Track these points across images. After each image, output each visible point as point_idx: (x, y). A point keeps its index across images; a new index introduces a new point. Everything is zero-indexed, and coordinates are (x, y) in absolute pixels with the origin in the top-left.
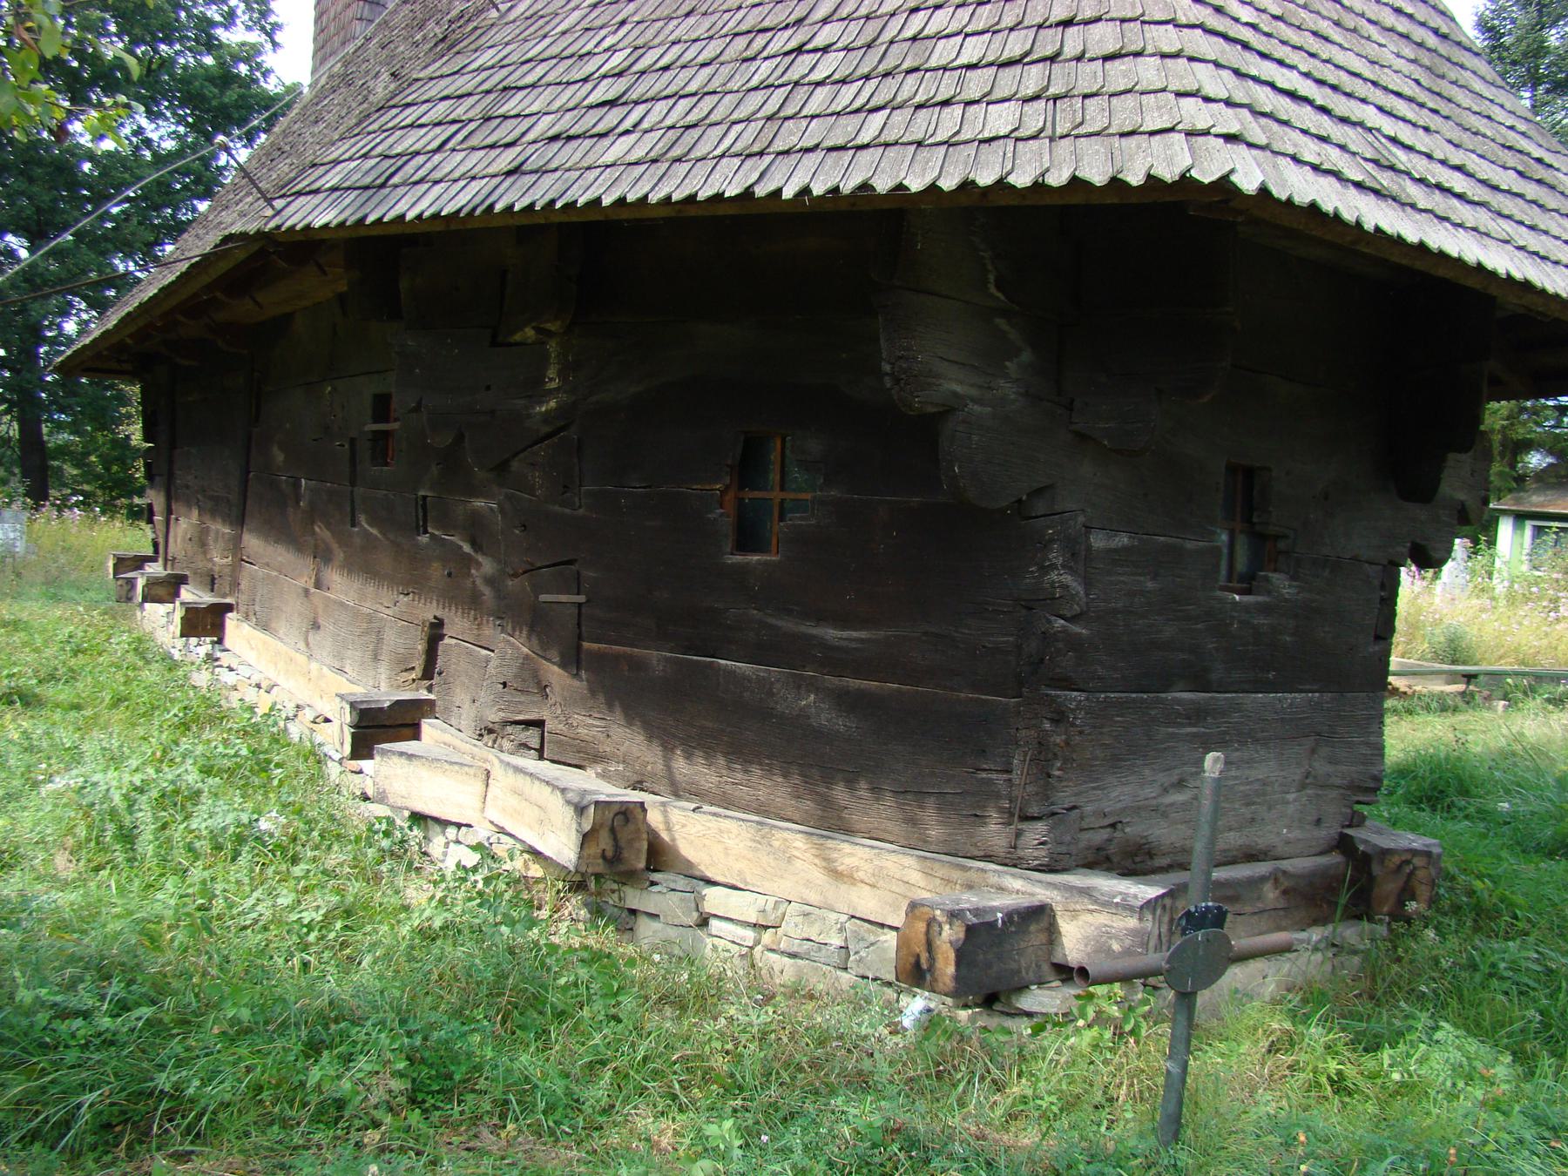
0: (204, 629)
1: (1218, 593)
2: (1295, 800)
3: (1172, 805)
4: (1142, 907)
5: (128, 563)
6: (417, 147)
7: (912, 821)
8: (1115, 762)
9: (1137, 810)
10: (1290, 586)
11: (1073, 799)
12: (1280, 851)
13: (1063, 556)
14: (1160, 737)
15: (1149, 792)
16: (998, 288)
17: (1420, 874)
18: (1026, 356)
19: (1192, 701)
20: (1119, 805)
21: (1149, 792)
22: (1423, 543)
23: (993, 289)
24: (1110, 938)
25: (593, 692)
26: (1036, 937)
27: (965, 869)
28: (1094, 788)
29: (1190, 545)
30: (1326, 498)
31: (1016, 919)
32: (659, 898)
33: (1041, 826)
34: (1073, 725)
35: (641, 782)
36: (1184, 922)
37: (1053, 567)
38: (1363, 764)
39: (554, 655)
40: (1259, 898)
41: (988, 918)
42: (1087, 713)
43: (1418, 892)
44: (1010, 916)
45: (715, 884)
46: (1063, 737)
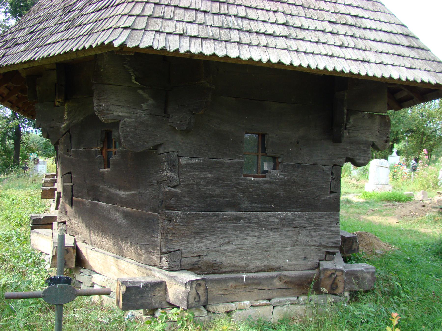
0: (49, 196)
1: (243, 177)
2: (290, 250)
3: (225, 250)
4: (186, 284)
5: (49, 176)
6: (45, 47)
7: (138, 253)
8: (196, 235)
9: (209, 251)
10: (280, 174)
11: (178, 247)
12: (286, 267)
13: (169, 166)
14: (218, 227)
15: (213, 245)
16: (136, 80)
17: (339, 278)
18: (151, 102)
19: (232, 215)
20: (199, 250)
21: (213, 245)
22: (352, 157)
23: (134, 81)
24: (179, 294)
25: (76, 213)
26: (158, 292)
27: (147, 269)
28: (187, 244)
29: (228, 161)
30: (298, 143)
31: (149, 285)
32: (82, 277)
33: (166, 256)
34: (175, 222)
35: (85, 241)
36: (50, 281)
37: (165, 170)
38: (327, 238)
39: (67, 201)
40: (271, 284)
41: (138, 285)
42: (181, 218)
43: (339, 285)
44: (146, 285)
45: (97, 273)
46: (172, 226)
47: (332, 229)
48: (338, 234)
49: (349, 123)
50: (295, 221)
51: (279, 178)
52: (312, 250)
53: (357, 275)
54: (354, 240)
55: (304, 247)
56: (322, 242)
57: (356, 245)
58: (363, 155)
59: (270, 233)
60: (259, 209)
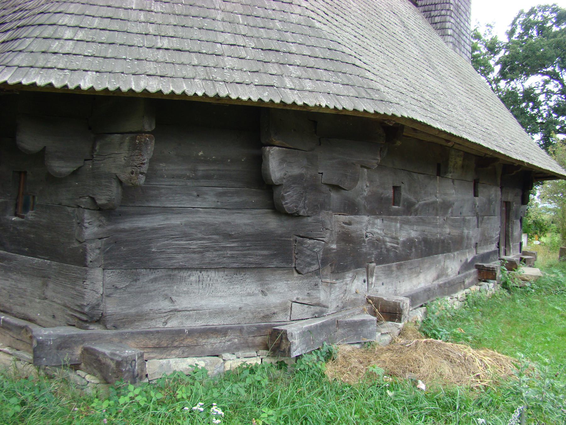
2: (39, 303)
47: (77, 288)
48: (83, 296)
49: (96, 151)
50: (45, 270)
51: (30, 219)
52: (58, 309)
53: (98, 357)
54: (284, 336)
55: (51, 303)
56: (66, 302)
57: (287, 345)
58: (104, 193)
59: (24, 279)
60: (17, 251)
